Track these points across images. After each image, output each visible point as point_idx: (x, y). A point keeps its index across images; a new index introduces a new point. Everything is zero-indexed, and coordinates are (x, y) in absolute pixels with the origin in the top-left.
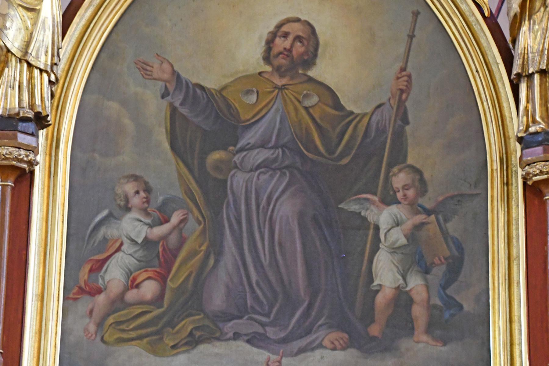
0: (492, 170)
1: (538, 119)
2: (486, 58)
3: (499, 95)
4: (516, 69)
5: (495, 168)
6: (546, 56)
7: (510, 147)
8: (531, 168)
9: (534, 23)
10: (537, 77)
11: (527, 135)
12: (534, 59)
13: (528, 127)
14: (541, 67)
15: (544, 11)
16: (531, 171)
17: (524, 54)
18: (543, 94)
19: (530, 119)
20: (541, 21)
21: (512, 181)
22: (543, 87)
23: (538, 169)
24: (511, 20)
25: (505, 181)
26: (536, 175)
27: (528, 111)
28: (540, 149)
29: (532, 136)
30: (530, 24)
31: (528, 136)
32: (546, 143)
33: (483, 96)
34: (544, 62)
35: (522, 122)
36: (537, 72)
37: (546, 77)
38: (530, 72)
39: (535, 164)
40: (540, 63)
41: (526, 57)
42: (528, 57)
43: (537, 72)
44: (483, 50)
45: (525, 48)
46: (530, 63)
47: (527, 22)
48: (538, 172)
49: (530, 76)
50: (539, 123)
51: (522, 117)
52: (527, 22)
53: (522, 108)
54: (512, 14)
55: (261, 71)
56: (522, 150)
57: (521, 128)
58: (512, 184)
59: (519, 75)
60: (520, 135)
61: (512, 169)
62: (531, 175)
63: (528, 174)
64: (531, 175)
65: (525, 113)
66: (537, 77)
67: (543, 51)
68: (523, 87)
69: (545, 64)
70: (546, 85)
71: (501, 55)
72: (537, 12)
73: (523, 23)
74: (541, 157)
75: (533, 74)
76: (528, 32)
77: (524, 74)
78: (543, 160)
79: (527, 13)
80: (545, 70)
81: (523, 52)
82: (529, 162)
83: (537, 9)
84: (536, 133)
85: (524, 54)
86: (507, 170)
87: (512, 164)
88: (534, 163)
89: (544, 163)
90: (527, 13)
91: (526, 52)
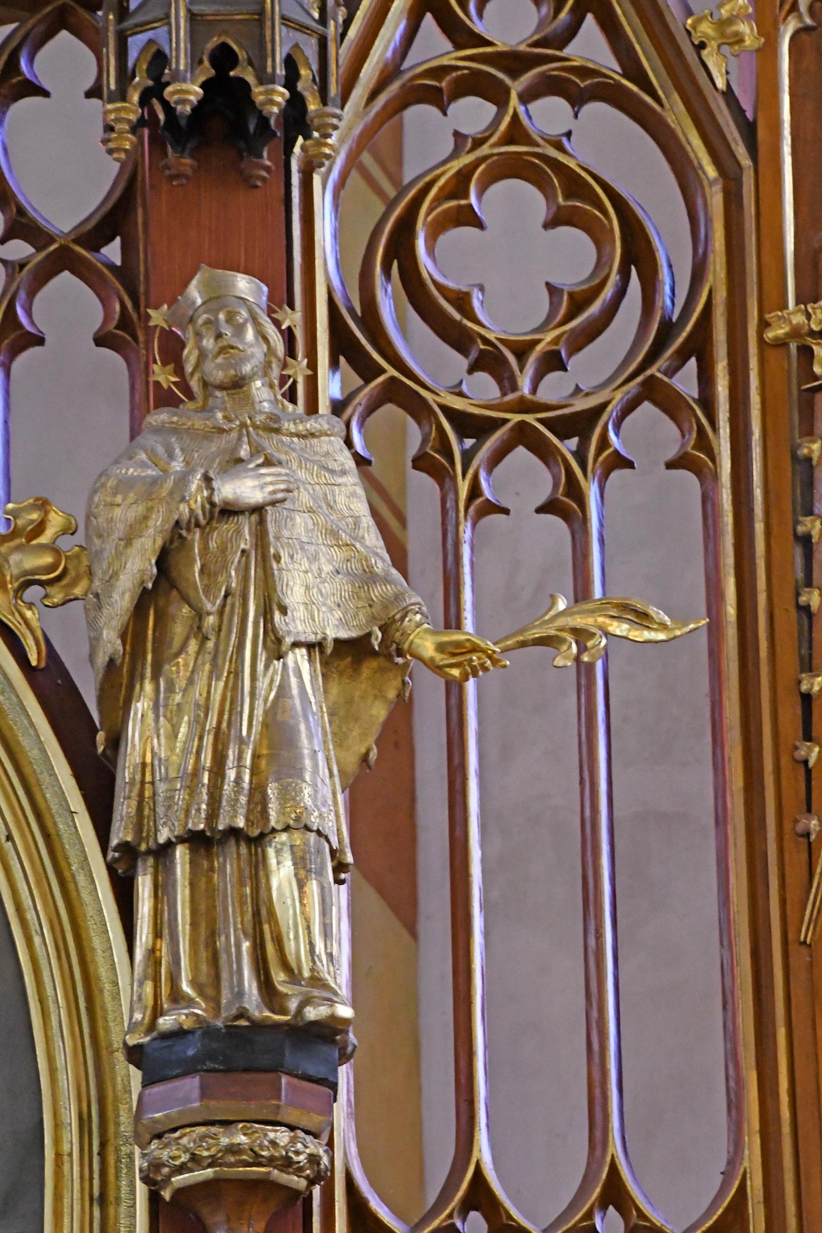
0: (58, 1156)
1: (186, 987)
2: (38, 797)
3: (78, 911)
4: (120, 833)
5: (66, 1148)
6: (205, 791)
7: (114, 1079)
8: (166, 1146)
9: (170, 689)
10: (181, 853)
11: (153, 1040)
12: (172, 798)
13: (157, 1012)
14: (190, 826)
15: (198, 653)
16: (165, 1155)
17: (143, 782)
18: (203, 907)
19: (165, 990)
20: (191, 681)
21: (118, 1188)
22: (202, 884)
23: (186, 1150)
24: (100, 676)
25: (96, 1193)
26: (181, 1169)
27: (157, 963)
28: (192, 1084)
29: (166, 1043)
30: (157, 690)
31: (157, 1044)
32: (210, 1065)
33: (30, 916)
34: (199, 810)
35: (140, 998)
36: (181, 840)
37: (209, 857)
38: (162, 840)
39: (177, 1134)
40: (187, 812)
41: (147, 794)
42: (154, 794)
43: (181, 840)
44: (27, 771)
45: (144, 765)
46: (160, 810)
47: (148, 687)
48: (184, 1158)
49: (164, 852)
50: (190, 1002)
51: (141, 984)
52: (148, 687)
53: (139, 954)
54: (102, 660)
55: (792, 538)
56: (146, 1084)
57: (138, 1016)
58: (118, 1200)
59: (129, 851)
60: (132, 1041)
61: (117, 1150)
62: (166, 1170)
63: (156, 1165)
64: (166, 1170)
65: (150, 971)
66: (181, 853)
67: (196, 773)
68: (144, 886)
69: (203, 815)
70: (210, 880)
71: (81, 789)
72: (178, 654)
73: (138, 687)
74: (194, 1111)
75: (169, 845)
76: (151, 715)
77: (143, 847)
78: (199, 1119)
79: (149, 657)
80: (203, 831)
81: (138, 777)
82: (160, 1128)
83: (176, 645)
84: (179, 1034)
85: (143, 782)
86: (102, 1154)
87: (117, 1135)
88: (175, 1130)
89: (202, 1130)
90: (149, 657)
91: (148, 778)
